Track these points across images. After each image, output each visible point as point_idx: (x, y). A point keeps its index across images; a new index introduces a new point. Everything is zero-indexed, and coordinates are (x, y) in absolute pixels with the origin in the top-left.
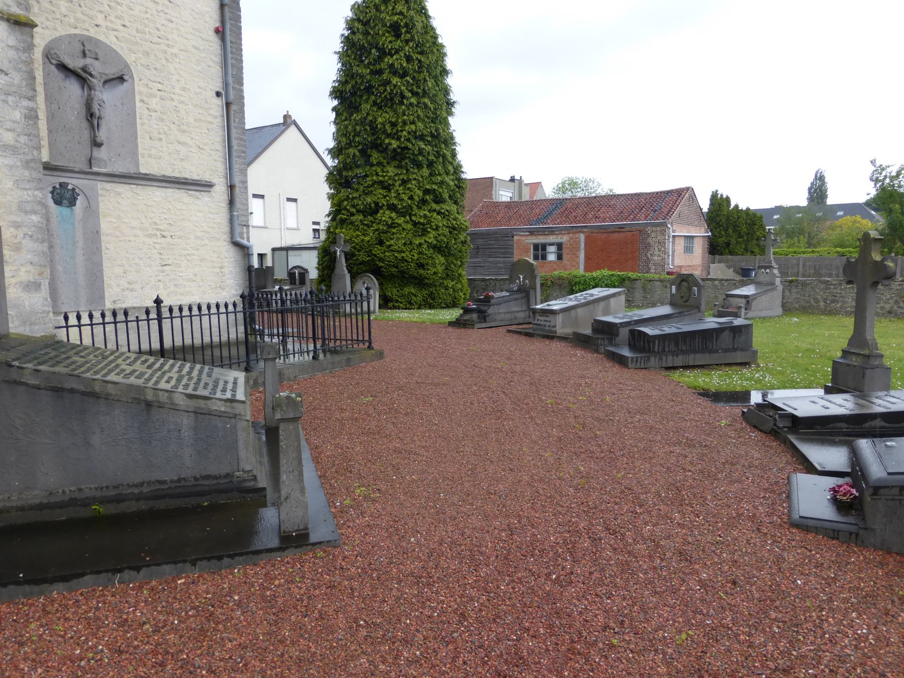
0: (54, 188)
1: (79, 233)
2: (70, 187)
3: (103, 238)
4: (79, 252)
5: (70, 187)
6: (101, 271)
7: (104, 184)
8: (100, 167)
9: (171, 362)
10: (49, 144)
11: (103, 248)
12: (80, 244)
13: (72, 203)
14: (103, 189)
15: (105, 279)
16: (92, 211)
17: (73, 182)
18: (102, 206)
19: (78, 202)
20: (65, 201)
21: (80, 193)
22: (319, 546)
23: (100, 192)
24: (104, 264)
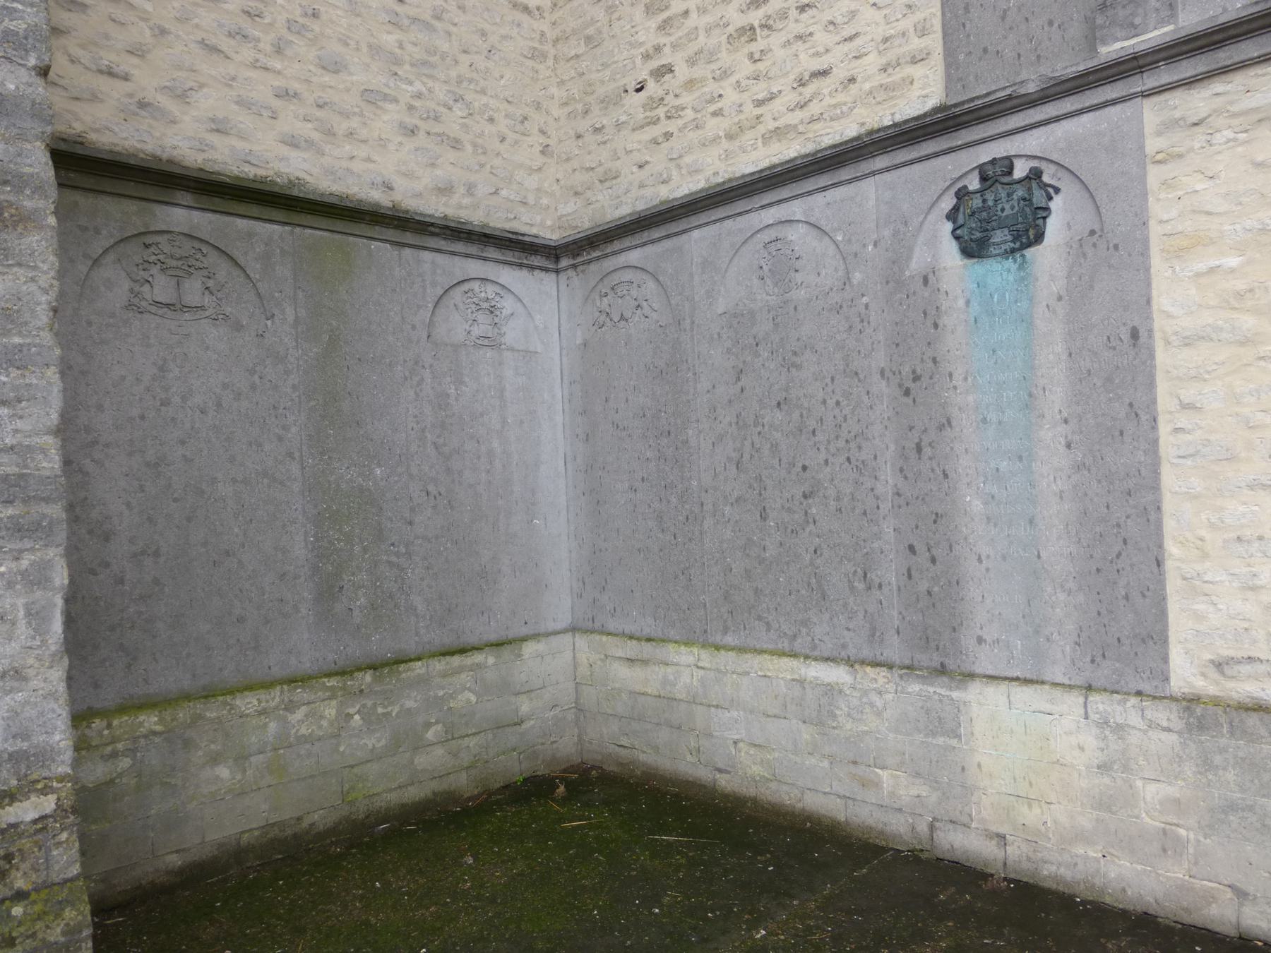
0: (962, 194)
1: (1052, 357)
2: (1020, 170)
3: (1162, 357)
4: (1051, 435)
5: (1020, 170)
6: (1151, 515)
7: (1176, 99)
8: (1134, 29)
9: (1178, 724)
10: (944, 25)
11: (1165, 401)
12: (1056, 398)
13: (1028, 232)
14: (1168, 126)
15: (1172, 549)
16: (1118, 251)
17: (1025, 146)
18: (1164, 212)
19: (1054, 227)
20: (999, 236)
21: (1065, 183)
22: (508, 647)
23: (1152, 144)
24: (1169, 479)
